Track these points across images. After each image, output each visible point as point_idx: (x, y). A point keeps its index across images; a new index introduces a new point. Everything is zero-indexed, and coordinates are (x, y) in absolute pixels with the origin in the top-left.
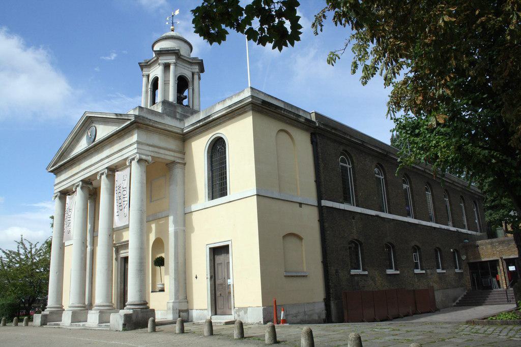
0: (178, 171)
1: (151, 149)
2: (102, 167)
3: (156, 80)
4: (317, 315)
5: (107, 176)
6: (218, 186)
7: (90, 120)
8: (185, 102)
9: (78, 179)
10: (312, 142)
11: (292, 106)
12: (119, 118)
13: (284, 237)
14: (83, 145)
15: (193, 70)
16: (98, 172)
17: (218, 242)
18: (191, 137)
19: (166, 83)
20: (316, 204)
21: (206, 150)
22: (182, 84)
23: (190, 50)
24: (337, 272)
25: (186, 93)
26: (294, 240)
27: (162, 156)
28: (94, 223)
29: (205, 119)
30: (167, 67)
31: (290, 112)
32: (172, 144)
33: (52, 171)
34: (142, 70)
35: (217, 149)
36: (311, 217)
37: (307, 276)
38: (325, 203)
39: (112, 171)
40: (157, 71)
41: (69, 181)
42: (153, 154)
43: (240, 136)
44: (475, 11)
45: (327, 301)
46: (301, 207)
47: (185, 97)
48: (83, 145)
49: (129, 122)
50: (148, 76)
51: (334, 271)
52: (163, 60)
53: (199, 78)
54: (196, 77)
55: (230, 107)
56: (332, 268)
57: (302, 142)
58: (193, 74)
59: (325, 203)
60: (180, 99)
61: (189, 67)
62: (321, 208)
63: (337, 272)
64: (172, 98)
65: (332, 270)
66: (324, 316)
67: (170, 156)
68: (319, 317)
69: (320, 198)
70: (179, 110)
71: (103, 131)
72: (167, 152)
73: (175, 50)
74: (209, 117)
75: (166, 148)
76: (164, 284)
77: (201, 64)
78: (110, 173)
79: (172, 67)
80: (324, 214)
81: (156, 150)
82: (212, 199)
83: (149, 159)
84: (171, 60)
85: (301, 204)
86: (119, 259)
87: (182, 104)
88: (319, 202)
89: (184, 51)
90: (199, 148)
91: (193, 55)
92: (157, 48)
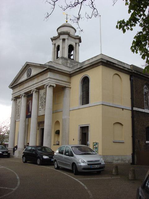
0: (67, 90)
1: (56, 81)
2: (33, 88)
3: (58, 47)
4: (127, 161)
5: (36, 92)
6: (85, 99)
7: (28, 66)
8: (72, 57)
9: (22, 92)
10: (130, 80)
11: (121, 62)
12: (41, 66)
13: (114, 124)
14: (25, 77)
15: (76, 42)
16: (45, 84)
17: (84, 124)
18: (74, 76)
19: (63, 48)
20: (131, 109)
21: (82, 79)
22: (71, 48)
23: (75, 32)
24: (139, 141)
25: (72, 53)
26: (119, 126)
27: (60, 84)
28: (62, 27)
29: (80, 68)
30: (64, 40)
31: (121, 66)
32: (65, 79)
33: (11, 88)
34: (52, 42)
35: (86, 81)
36: (129, 114)
37: (123, 143)
38: (135, 109)
39: (38, 89)
40: (59, 42)
41: (18, 93)
42: (57, 83)
43: (97, 77)
44: (46, 159)
45: (133, 155)
46: (123, 110)
47: (72, 55)
48: (25, 77)
49: (46, 69)
50: (55, 44)
51: (138, 141)
52: (62, 37)
53: (79, 45)
54: (77, 45)
55: (91, 63)
56: (137, 140)
57: (126, 80)
58: (76, 44)
59: (135, 109)
60: (70, 56)
61: (74, 40)
62: (133, 111)
63: (139, 141)
64: (66, 55)
65: (136, 140)
66: (131, 162)
67: (63, 84)
68: (128, 162)
69: (133, 106)
70: (69, 61)
71: (34, 72)
72: (63, 82)
73: (68, 32)
74: (82, 67)
75: (61, 80)
76: (59, 142)
77: (80, 39)
78: (37, 90)
79: (66, 40)
80: (134, 114)
81: (58, 81)
82: (82, 105)
83: (55, 85)
84: (65, 37)
85: (123, 109)
86: (40, 129)
87: (70, 58)
88: (132, 108)
89: (72, 32)
90: (77, 81)
91: (76, 34)
92: (59, 31)
